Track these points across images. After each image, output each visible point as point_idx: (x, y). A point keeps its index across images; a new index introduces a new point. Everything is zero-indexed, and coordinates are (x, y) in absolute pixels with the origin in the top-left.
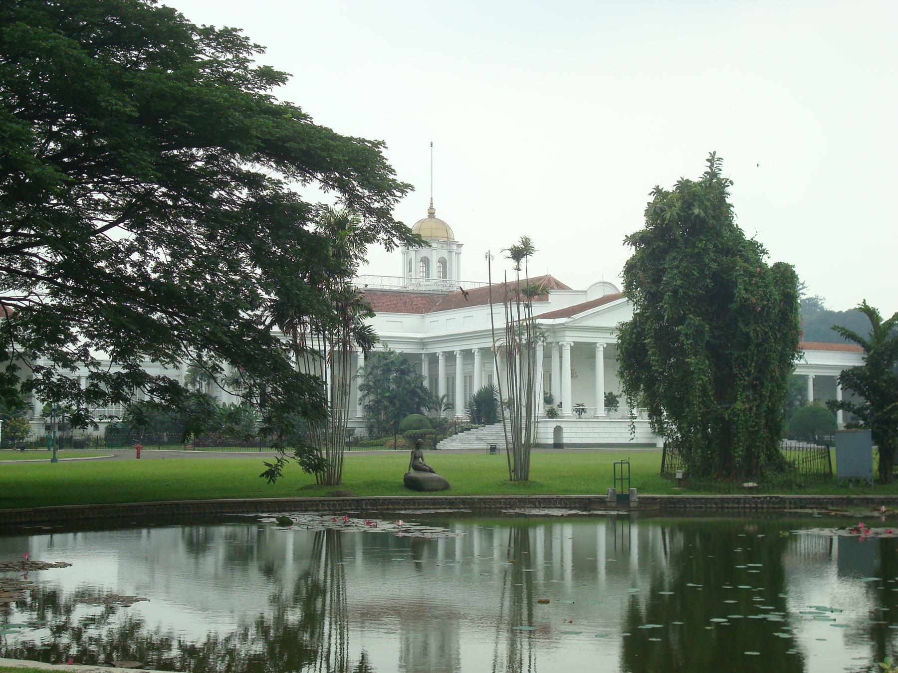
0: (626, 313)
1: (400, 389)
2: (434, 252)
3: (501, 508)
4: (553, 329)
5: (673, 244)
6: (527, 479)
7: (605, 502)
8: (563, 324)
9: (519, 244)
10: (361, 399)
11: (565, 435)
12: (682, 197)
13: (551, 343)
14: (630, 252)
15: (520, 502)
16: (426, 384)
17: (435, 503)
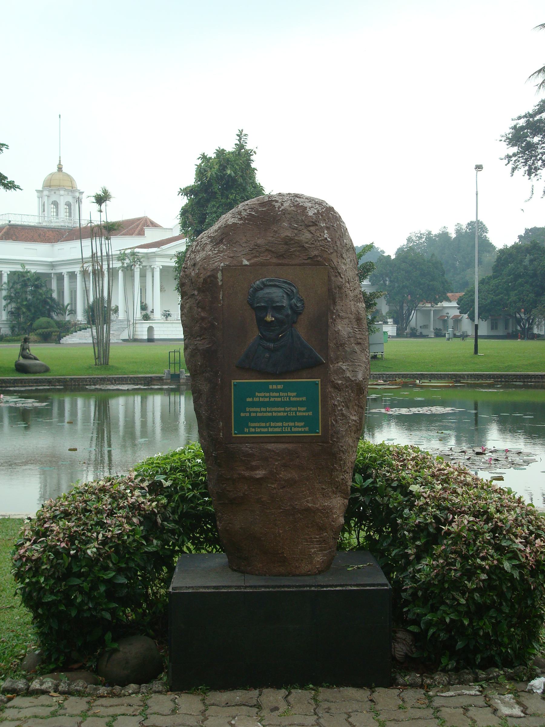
0: (181, 246)
1: (35, 299)
2: (62, 197)
3: (87, 385)
4: (147, 256)
5: (213, 195)
6: (108, 364)
7: (163, 380)
8: (154, 253)
9: (100, 193)
10: (5, 307)
11: (155, 333)
12: (220, 162)
13: (146, 266)
14: (184, 201)
15: (101, 380)
16: (55, 295)
17: (38, 382)
